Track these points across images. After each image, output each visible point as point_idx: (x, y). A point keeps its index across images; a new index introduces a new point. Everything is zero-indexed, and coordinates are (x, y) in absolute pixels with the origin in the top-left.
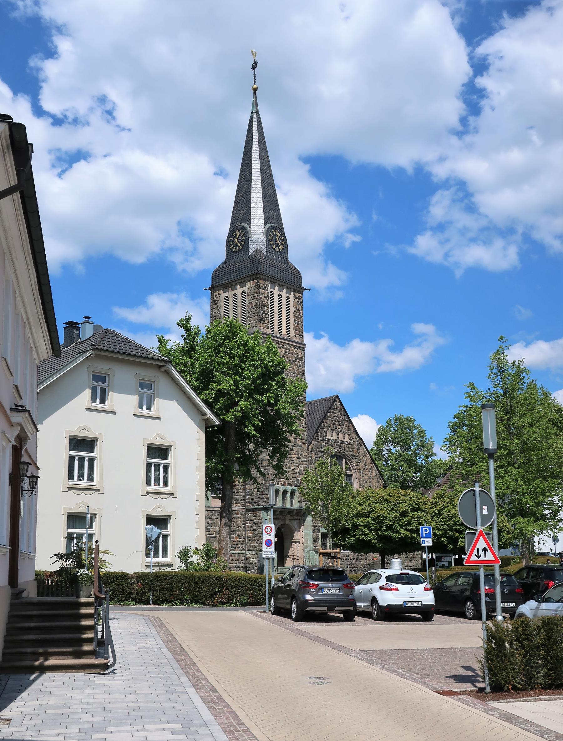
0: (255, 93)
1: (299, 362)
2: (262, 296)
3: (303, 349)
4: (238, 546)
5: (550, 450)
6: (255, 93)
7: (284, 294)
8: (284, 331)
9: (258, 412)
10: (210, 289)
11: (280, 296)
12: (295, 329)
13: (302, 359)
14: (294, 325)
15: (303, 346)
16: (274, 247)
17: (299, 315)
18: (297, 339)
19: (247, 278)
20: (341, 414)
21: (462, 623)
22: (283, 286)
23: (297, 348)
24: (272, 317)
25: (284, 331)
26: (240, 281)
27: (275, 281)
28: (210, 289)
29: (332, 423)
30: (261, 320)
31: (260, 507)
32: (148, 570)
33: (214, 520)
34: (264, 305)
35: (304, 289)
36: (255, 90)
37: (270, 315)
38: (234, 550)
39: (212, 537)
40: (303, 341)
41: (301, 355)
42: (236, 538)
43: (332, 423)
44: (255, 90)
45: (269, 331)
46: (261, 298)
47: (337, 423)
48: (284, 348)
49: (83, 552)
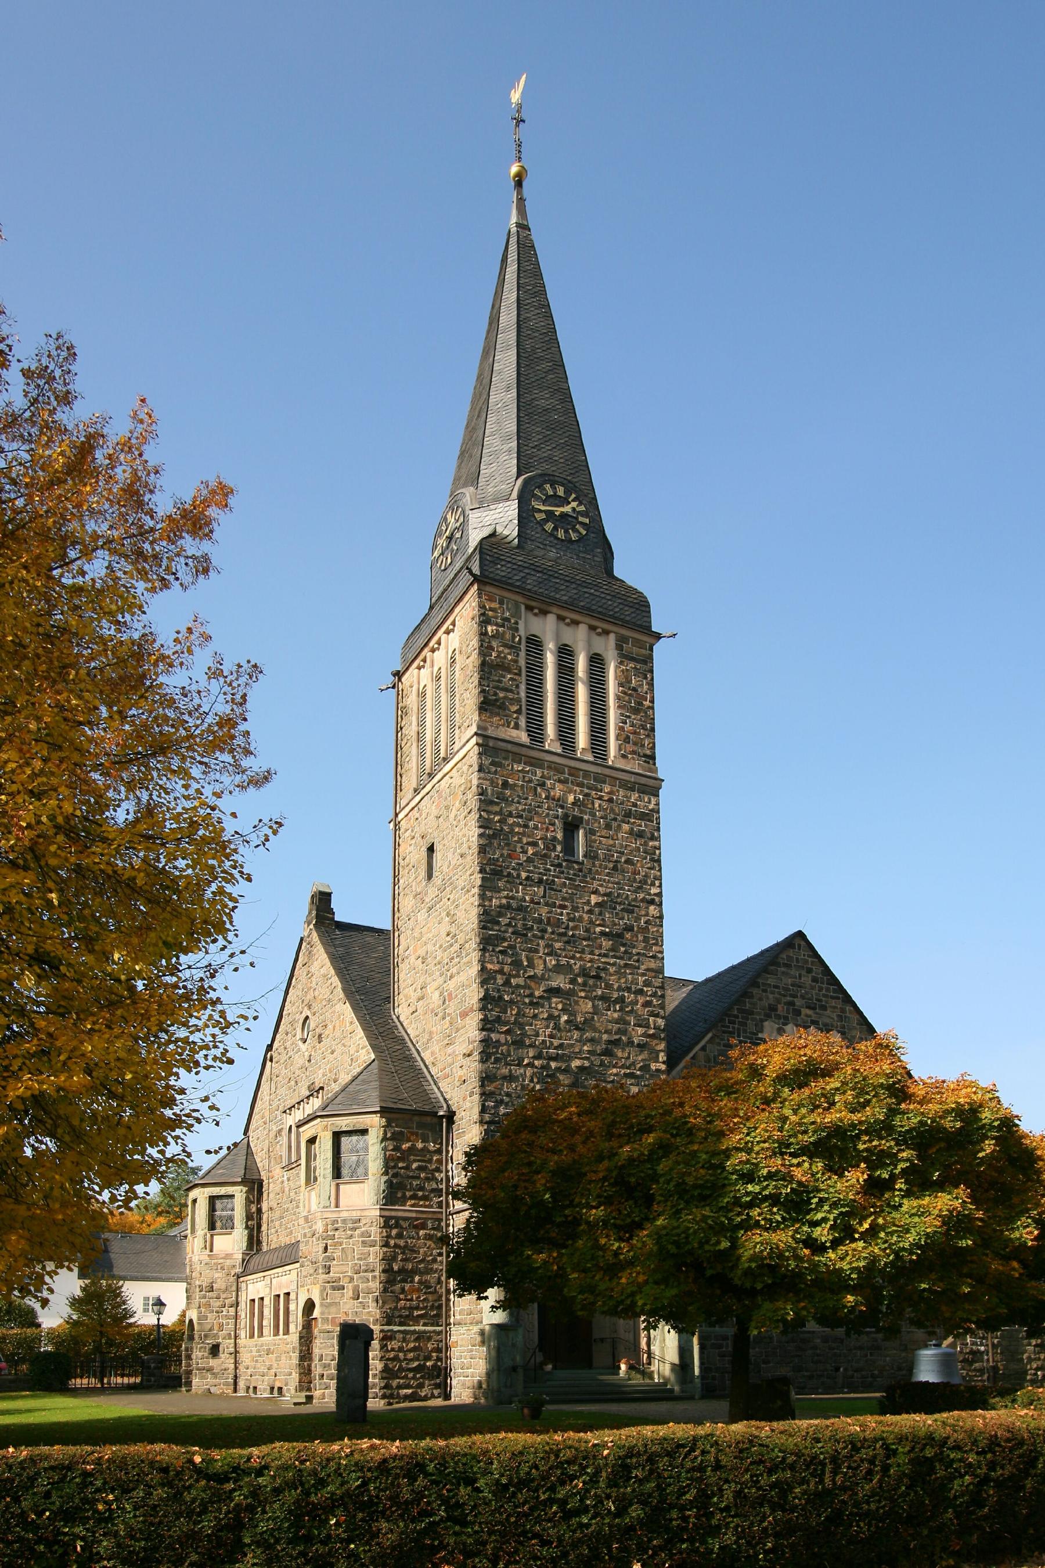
3: (655, 792)
5: (422, 1233)
7: (579, 638)
8: (582, 740)
9: (75, 438)
11: (565, 654)
13: (652, 816)
15: (651, 782)
16: (561, 534)
18: (634, 765)
20: (815, 980)
21: (44, 1397)
25: (582, 740)
26: (443, 629)
27: (544, 607)
29: (784, 1000)
35: (658, 637)
37: (523, 694)
39: (334, 1288)
43: (784, 1000)
47: (798, 1002)
49: (690, 1180)
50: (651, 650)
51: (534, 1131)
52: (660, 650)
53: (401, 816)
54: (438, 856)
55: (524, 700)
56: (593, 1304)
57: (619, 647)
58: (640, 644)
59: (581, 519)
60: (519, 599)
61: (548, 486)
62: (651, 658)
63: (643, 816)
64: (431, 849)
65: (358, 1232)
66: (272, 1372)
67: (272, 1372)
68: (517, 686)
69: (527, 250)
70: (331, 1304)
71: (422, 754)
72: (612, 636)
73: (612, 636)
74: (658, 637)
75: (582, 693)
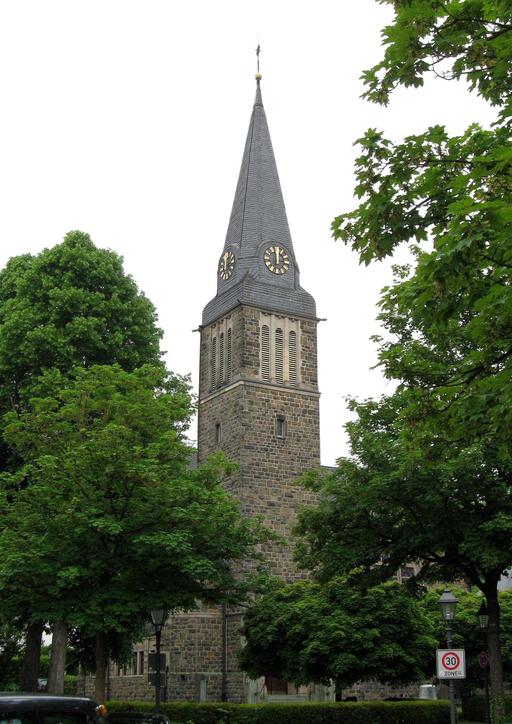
0: (258, 83)
1: (308, 417)
2: (249, 333)
4: (213, 665)
6: (258, 83)
8: (286, 376)
10: (199, 330)
12: (303, 373)
13: (316, 413)
14: (302, 368)
15: (315, 395)
16: (272, 269)
17: (310, 354)
19: (232, 312)
22: (283, 317)
23: (305, 398)
24: (266, 359)
25: (286, 376)
28: (199, 330)
30: (244, 363)
31: (240, 612)
32: (388, 704)
33: (179, 631)
34: (250, 344)
35: (319, 320)
36: (258, 79)
38: (205, 671)
39: (176, 653)
40: (317, 388)
41: (312, 407)
42: (210, 654)
44: (258, 79)
45: (259, 377)
46: (247, 335)
48: (284, 399)
50: (316, 326)
51: (94, 417)
52: (320, 326)
53: (202, 402)
54: (221, 432)
55: (261, 360)
56: (477, 637)
57: (302, 327)
58: (310, 324)
59: (285, 262)
60: (259, 310)
61: (271, 248)
62: (316, 330)
63: (310, 412)
64: (218, 426)
65: (187, 625)
66: (133, 695)
67: (133, 695)
68: (257, 353)
69: (259, 105)
70: (174, 661)
71: (213, 372)
72: (299, 322)
73: (299, 322)
74: (319, 320)
75: (286, 352)
